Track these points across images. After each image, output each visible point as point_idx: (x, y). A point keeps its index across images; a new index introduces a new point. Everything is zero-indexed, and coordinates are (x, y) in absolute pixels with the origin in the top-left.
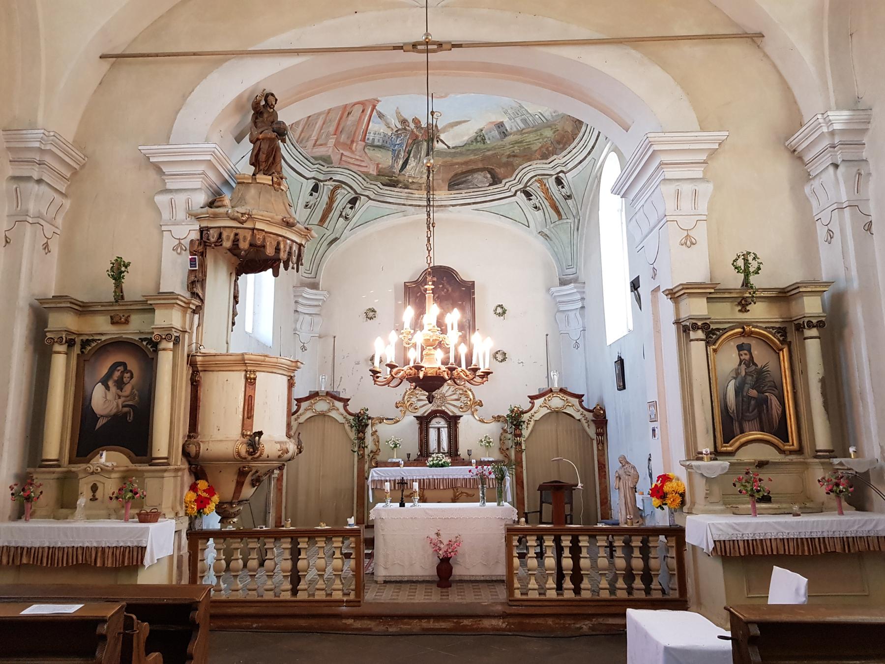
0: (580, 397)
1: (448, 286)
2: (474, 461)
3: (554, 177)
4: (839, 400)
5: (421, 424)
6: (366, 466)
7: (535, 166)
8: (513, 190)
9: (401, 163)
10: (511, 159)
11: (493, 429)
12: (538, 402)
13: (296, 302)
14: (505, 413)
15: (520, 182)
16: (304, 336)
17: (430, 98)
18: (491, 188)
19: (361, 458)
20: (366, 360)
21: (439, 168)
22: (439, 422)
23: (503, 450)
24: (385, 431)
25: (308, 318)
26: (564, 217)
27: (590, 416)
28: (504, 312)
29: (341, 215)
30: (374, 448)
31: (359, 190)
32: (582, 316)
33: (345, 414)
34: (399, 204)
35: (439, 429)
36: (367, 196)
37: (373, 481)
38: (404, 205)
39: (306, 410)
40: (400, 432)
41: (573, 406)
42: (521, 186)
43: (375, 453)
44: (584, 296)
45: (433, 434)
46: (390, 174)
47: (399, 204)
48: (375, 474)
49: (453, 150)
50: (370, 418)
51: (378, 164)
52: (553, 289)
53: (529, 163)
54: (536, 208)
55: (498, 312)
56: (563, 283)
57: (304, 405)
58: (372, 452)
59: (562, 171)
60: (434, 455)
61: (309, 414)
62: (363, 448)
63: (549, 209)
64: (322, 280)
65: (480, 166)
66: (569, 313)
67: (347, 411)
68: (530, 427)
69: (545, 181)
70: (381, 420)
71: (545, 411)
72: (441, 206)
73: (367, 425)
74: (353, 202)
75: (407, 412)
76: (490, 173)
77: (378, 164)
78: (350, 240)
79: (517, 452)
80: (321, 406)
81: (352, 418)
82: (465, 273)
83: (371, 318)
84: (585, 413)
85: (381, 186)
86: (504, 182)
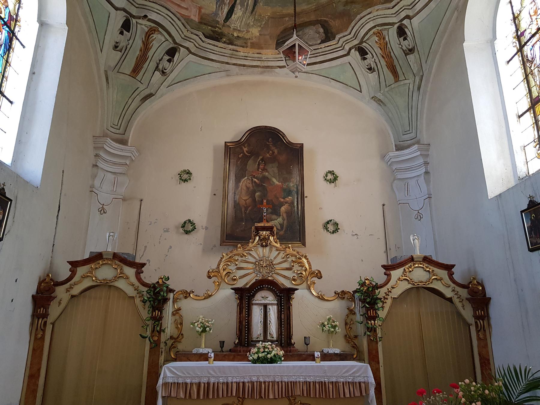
0: (449, 268)
1: (273, 148)
2: (317, 354)
3: (396, 26)
4: (281, 321)
5: (241, 299)
6: (162, 359)
7: (375, 14)
8: (347, 47)
9: (226, 10)
10: (348, 7)
11: (335, 308)
12: (396, 274)
13: (97, 156)
14: (352, 286)
15: (355, 36)
16: (104, 197)
17: (234, 56)
18: (323, 45)
19: (155, 346)
20: (177, 228)
21: (268, 20)
22: (265, 297)
23: (350, 338)
24: (192, 309)
25: (110, 176)
26: (401, 77)
27: (464, 293)
28: (336, 178)
29: (157, 68)
30: (176, 334)
31: (178, 40)
32: (427, 182)
33: (137, 283)
34: (222, 62)
35: (265, 306)
36: (187, 49)
37: (165, 384)
38: (227, 63)
39: (84, 277)
40: (210, 309)
41: (441, 279)
42: (356, 42)
43: (176, 339)
44: (428, 160)
45: (257, 314)
46: (213, 24)
47: (222, 62)
48: (169, 374)
49: (225, 353)
50: (172, 291)
51: (200, 9)
52: (391, 154)
53: (369, 10)
54: (370, 69)
56: (399, 148)
57: (81, 271)
58: (171, 338)
59: (408, 17)
60: (260, 345)
61: (87, 283)
62: (159, 332)
63: (385, 69)
64: (131, 135)
65: (313, 18)
68: (387, 306)
69: (385, 33)
70: (187, 294)
71: (405, 286)
72: (268, 67)
73: (166, 300)
74: (172, 52)
75: (223, 285)
76: (323, 26)
77: (200, 9)
78: (166, 98)
79: (370, 342)
80: (105, 272)
81: (145, 289)
82: (294, 134)
83: (185, 181)
84: (458, 289)
85: (204, 38)
86: (338, 37)
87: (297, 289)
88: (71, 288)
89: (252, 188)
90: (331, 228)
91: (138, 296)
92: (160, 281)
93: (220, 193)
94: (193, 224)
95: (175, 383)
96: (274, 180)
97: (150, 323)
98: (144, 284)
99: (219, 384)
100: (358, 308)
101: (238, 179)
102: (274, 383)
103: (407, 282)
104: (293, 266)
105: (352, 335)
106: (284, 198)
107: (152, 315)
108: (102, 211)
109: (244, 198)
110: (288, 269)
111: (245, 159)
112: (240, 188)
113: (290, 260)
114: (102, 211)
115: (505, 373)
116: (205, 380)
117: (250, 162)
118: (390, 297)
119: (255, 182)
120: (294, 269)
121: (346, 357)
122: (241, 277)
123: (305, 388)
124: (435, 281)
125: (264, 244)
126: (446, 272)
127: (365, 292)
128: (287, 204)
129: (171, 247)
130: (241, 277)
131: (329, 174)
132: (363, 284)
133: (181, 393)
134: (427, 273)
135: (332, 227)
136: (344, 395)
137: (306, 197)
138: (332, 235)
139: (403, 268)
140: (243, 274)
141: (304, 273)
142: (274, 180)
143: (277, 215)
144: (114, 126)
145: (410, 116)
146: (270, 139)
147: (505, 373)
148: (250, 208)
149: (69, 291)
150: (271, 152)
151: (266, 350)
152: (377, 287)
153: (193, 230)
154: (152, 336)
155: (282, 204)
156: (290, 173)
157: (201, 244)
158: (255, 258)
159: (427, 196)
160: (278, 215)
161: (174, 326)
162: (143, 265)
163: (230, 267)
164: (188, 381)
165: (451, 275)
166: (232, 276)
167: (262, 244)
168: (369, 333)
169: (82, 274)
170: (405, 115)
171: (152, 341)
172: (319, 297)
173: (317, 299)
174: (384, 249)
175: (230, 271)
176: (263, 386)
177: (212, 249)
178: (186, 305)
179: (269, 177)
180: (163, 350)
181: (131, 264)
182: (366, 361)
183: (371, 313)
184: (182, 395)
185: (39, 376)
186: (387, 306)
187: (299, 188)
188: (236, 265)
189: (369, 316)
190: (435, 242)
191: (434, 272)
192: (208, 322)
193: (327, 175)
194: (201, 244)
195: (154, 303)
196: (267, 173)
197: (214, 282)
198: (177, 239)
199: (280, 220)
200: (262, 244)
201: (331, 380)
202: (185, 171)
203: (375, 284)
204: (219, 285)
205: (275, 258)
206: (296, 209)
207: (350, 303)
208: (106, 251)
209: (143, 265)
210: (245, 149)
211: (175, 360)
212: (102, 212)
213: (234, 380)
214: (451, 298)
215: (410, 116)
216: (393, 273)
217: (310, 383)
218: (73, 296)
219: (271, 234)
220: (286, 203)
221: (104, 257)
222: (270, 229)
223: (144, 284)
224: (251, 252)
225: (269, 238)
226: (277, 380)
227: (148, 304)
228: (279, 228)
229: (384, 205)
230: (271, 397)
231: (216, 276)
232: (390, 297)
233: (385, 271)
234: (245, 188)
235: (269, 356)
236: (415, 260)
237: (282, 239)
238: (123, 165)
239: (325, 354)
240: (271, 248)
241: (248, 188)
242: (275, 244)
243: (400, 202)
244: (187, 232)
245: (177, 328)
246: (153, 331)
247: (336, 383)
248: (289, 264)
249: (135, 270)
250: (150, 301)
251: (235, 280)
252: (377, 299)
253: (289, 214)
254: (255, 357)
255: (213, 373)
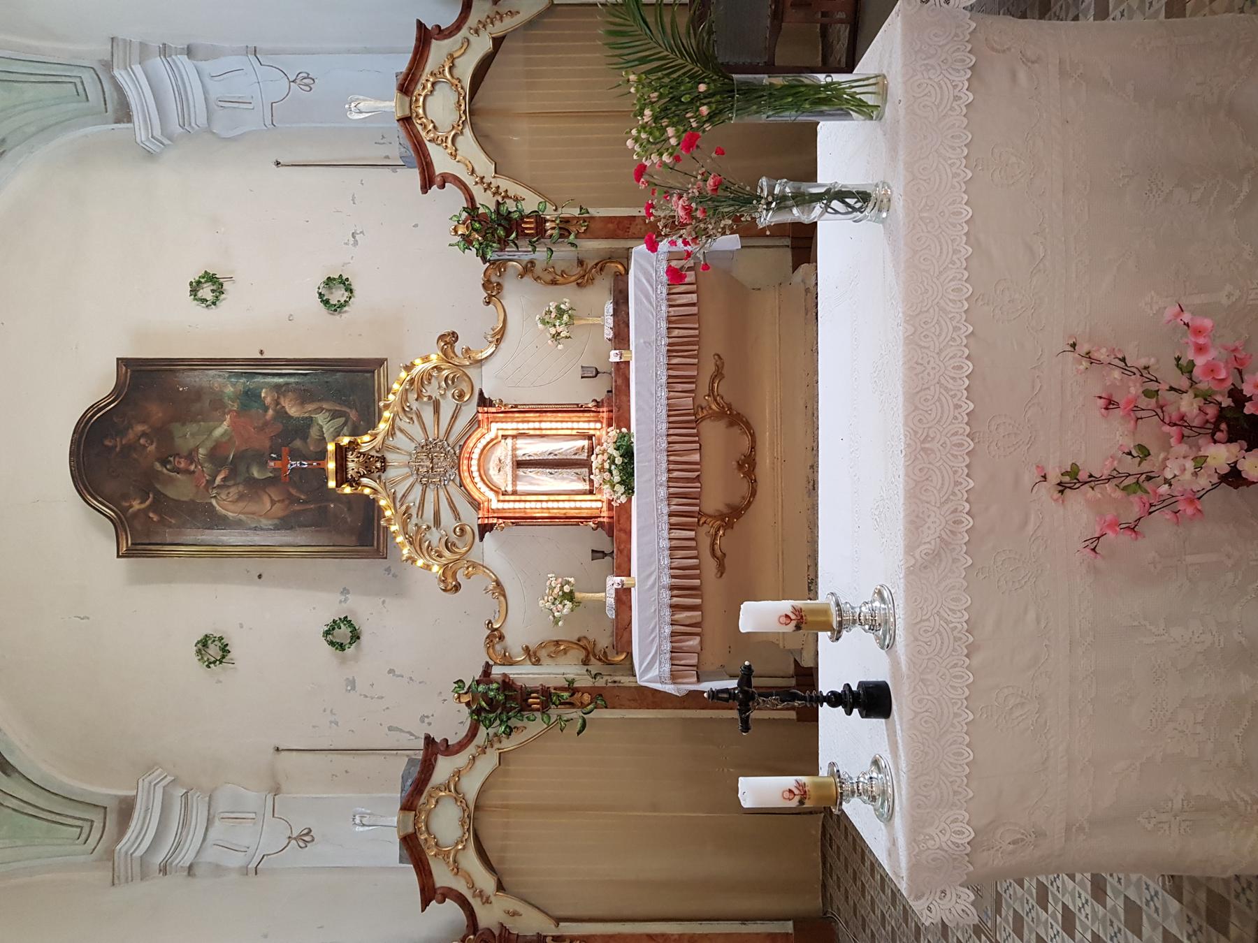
0: (425, 36)
1: (131, 435)
2: (614, 357)
6: (626, 681)
12: (441, 162)
13: (164, 870)
14: (472, 266)
16: (270, 838)
19: (601, 697)
20: (343, 661)
23: (584, 275)
28: (211, 278)
32: (213, 53)
33: (471, 749)
37: (674, 678)
39: (457, 870)
41: (452, 58)
43: (589, 653)
44: (155, 44)
48: (654, 672)
50: (487, 672)
52: (141, 135)
55: (210, 296)
56: (124, 114)
57: (442, 877)
58: (585, 662)
61: (471, 861)
64: (106, 790)
66: (213, 96)
67: (462, 746)
68: (515, 189)
70: (495, 636)
71: (467, 141)
73: (507, 684)
75: (473, 556)
79: (589, 234)
80: (446, 823)
81: (483, 732)
82: (94, 383)
83: (225, 650)
84: (472, 20)
87: (481, 393)
88: (481, 894)
89: (241, 488)
90: (338, 295)
91: (497, 745)
92: (466, 699)
93: (255, 565)
94: (334, 625)
95: (672, 659)
96: (218, 432)
97: (554, 712)
98: (473, 733)
99: (673, 565)
100: (520, 254)
101: (220, 522)
102: (670, 453)
103: (460, 139)
104: (430, 398)
105: (578, 271)
106: (266, 409)
107: (538, 710)
108: (305, 838)
109: (268, 505)
110: (437, 410)
111: (162, 505)
112: (242, 517)
113: (415, 405)
114: (305, 838)
115: (620, 56)
116: (666, 594)
117: (171, 492)
118: (493, 181)
119: (224, 479)
120: (435, 395)
121: (620, 292)
122: (457, 516)
123: (680, 387)
124: (456, 72)
125: (378, 465)
126: (435, 44)
127: (483, 237)
128: (282, 401)
129: (391, 671)
130: (457, 516)
131: (200, 294)
132: (467, 241)
133: (691, 643)
134: (437, 87)
135: (336, 292)
136: (693, 305)
137: (261, 352)
138: (355, 293)
139: (428, 144)
140: (450, 511)
141: (445, 373)
142: (218, 432)
143: (309, 426)
144: (84, 836)
145: (32, 78)
146: (107, 443)
147: (620, 56)
148: (293, 492)
149: (488, 898)
150: (142, 441)
151: (607, 466)
152: (472, 208)
153: (350, 623)
154: (583, 706)
155: (282, 414)
156: (197, 394)
157: (384, 602)
158: (412, 486)
159: (252, 58)
160: (309, 422)
161: (561, 659)
162: (429, 741)
163: (435, 543)
164: (667, 630)
165: (442, 33)
166: (453, 538)
167: (379, 470)
168: (572, 237)
169: (450, 875)
170: (30, 92)
171: (591, 706)
172: (498, 341)
173: (502, 345)
174: (387, 171)
175: (443, 541)
176: (675, 474)
177: (395, 576)
178: (517, 636)
179: (210, 444)
180: (610, 679)
181: (427, 767)
182: (628, 243)
183: (529, 226)
184: (694, 642)
185: (663, 935)
186: (515, 189)
187: (238, 370)
188: (429, 527)
189: (537, 234)
190: (367, 51)
191: (436, 71)
192: (552, 589)
193: (204, 300)
194: (384, 602)
195: (512, 709)
196: (201, 450)
197: (468, 576)
198: (372, 656)
199: (321, 418)
200: (379, 470)
201: (664, 331)
202: (199, 652)
203: (465, 215)
204: (474, 565)
205: (412, 439)
206: (292, 380)
207: (510, 271)
208: (398, 827)
209: (429, 741)
210: (137, 505)
211: (630, 655)
212: (306, 838)
213: (665, 534)
214: (494, 39)
215: (32, 78)
216: (438, 170)
217: (669, 377)
218: (500, 887)
219: (354, 450)
220: (278, 403)
221: (411, 830)
222: (341, 453)
223: (473, 733)
224: (399, 496)
225: (364, 454)
226: (665, 445)
227: (514, 722)
228: (342, 420)
229: (278, 164)
230: (696, 457)
231: (455, 574)
232: (493, 181)
233: (435, 187)
234: (241, 505)
235: (618, 461)
236: (407, 113)
237: (369, 420)
238: (186, 804)
239: (616, 336)
240: (390, 449)
241: (241, 497)
242: (380, 438)
243: (268, 122)
244: (355, 636)
245: (565, 651)
246: (572, 705)
247: (670, 322)
248: (425, 407)
249: (440, 757)
250: (509, 719)
251: (462, 530)
252: (498, 211)
253: (305, 396)
254: (620, 489)
255: (653, 578)
